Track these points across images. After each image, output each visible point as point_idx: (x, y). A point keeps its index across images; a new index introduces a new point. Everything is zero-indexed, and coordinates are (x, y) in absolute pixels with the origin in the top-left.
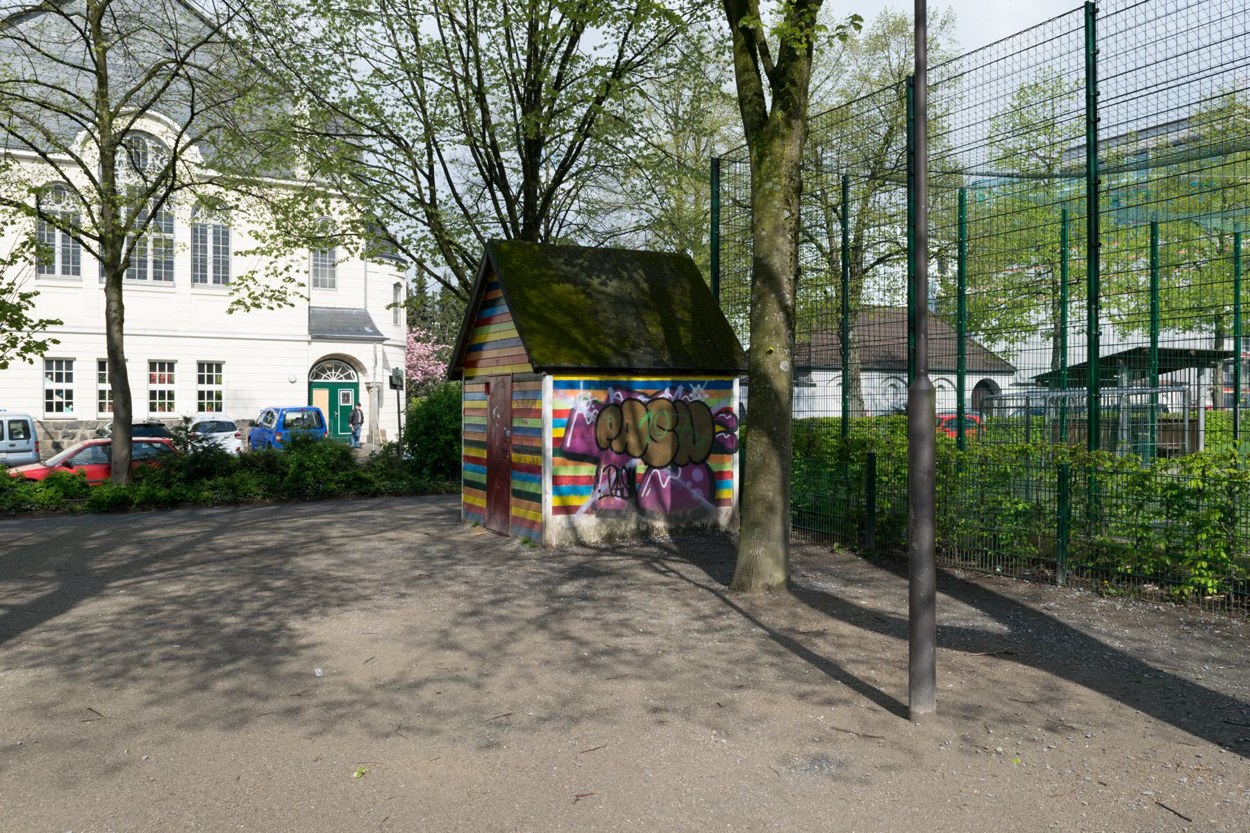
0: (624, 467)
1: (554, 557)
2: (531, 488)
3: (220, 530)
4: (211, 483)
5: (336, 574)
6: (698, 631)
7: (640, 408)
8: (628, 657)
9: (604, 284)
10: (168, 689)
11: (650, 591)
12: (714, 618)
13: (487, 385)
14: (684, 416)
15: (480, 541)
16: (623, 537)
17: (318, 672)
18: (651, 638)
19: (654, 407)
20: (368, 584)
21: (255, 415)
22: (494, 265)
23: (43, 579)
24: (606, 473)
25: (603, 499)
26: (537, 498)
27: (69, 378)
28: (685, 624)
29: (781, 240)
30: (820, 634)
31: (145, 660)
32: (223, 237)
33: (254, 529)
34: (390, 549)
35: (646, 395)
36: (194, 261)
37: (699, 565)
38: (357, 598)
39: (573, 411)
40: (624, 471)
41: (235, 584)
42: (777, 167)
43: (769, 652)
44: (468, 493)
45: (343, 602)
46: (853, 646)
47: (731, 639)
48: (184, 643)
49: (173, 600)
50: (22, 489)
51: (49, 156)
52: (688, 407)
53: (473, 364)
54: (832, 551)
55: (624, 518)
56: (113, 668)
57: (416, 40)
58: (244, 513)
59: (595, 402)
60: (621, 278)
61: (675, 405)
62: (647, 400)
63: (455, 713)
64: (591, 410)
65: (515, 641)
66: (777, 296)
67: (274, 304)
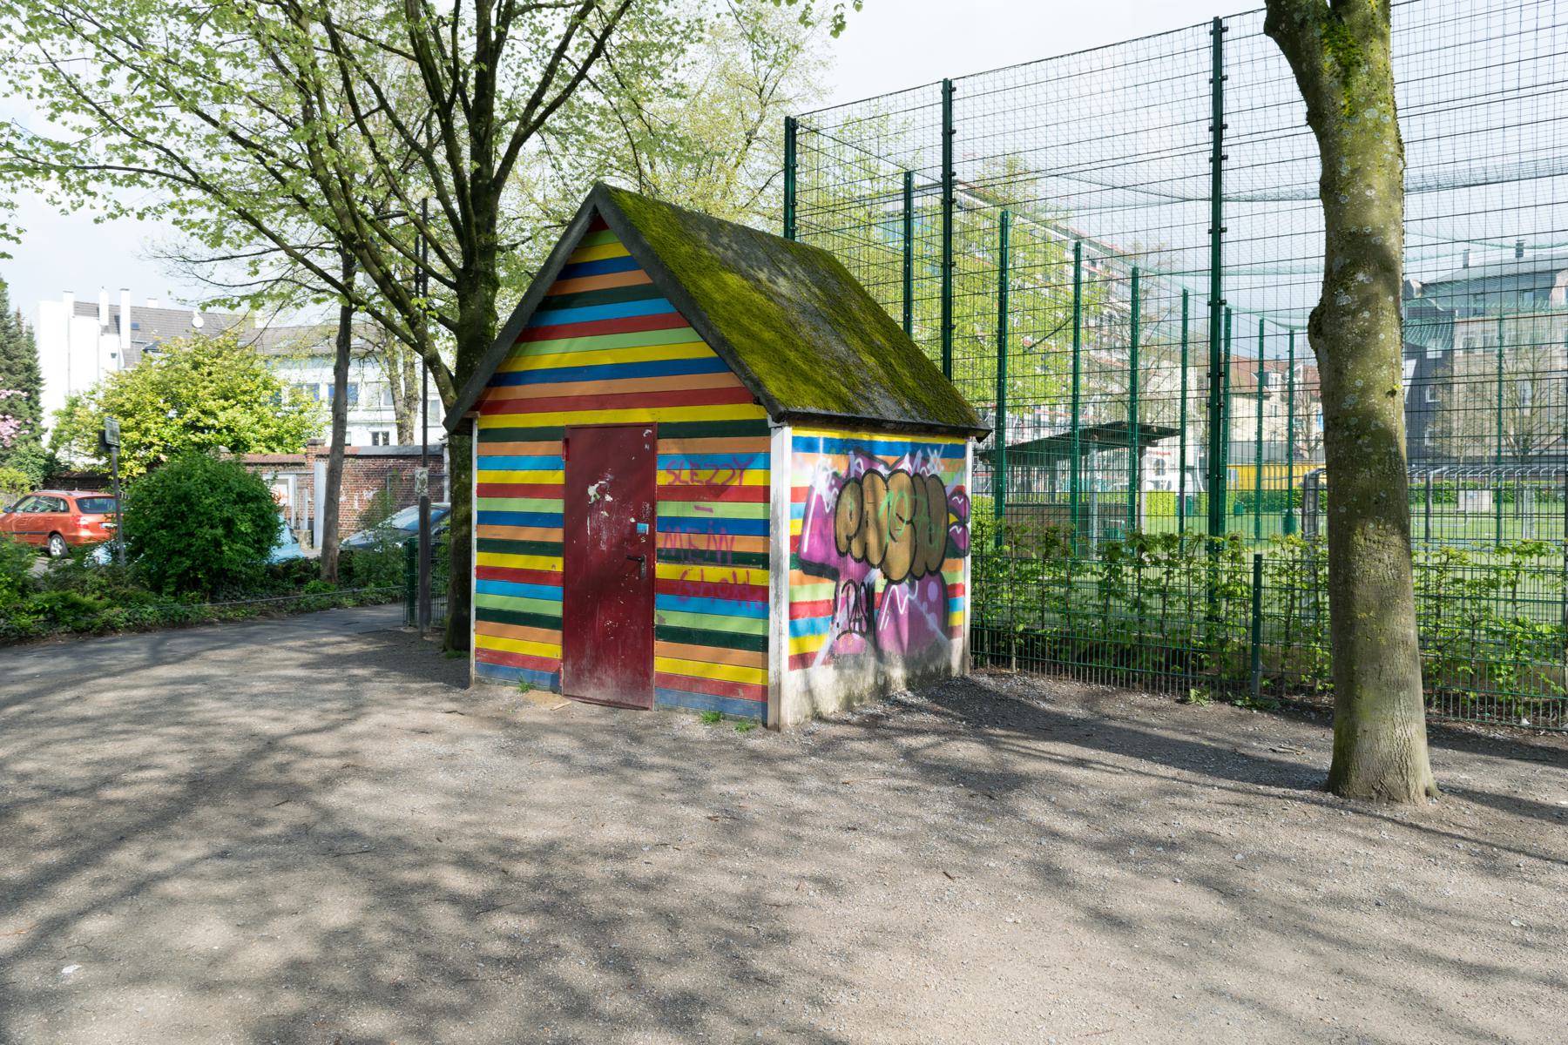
0: (863, 584)
39: (811, 488)
64: (831, 487)
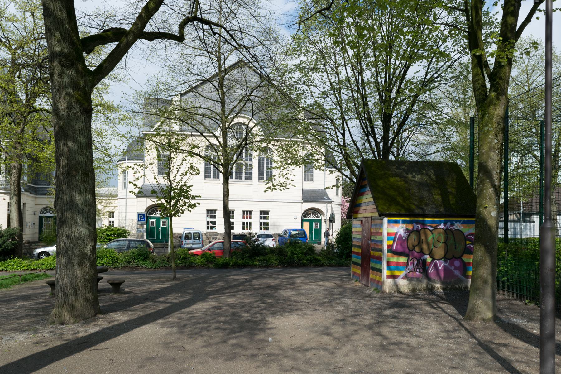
1: (387, 297)
2: (378, 266)
3: (256, 278)
4: (258, 258)
5: (293, 298)
6: (442, 338)
7: (429, 232)
8: (404, 347)
9: (414, 177)
10: (212, 341)
11: (425, 316)
12: (452, 332)
13: (362, 221)
15: (357, 288)
16: (420, 290)
17: (270, 340)
18: (418, 338)
19: (436, 232)
20: (304, 304)
21: (280, 232)
22: (364, 170)
23: (188, 293)
26: (380, 271)
27: (215, 217)
28: (437, 334)
29: (493, 154)
30: (505, 345)
31: (209, 328)
32: (270, 161)
33: (269, 278)
34: (318, 289)
35: (432, 227)
36: (259, 172)
37: (454, 306)
38: (297, 310)
39: (397, 233)
41: (253, 300)
42: (491, 119)
43: (475, 352)
44: (354, 267)
45: (291, 311)
46: (521, 353)
47: (458, 343)
48: (225, 323)
49: (228, 305)
50: (192, 258)
51: (204, 134)
53: (357, 212)
54: (525, 304)
55: (421, 282)
56: (197, 331)
57: (338, 77)
58: (269, 271)
59: (407, 229)
60: (422, 174)
61: (446, 231)
63: (318, 364)
64: (405, 233)
65: (356, 334)
67: (282, 188)
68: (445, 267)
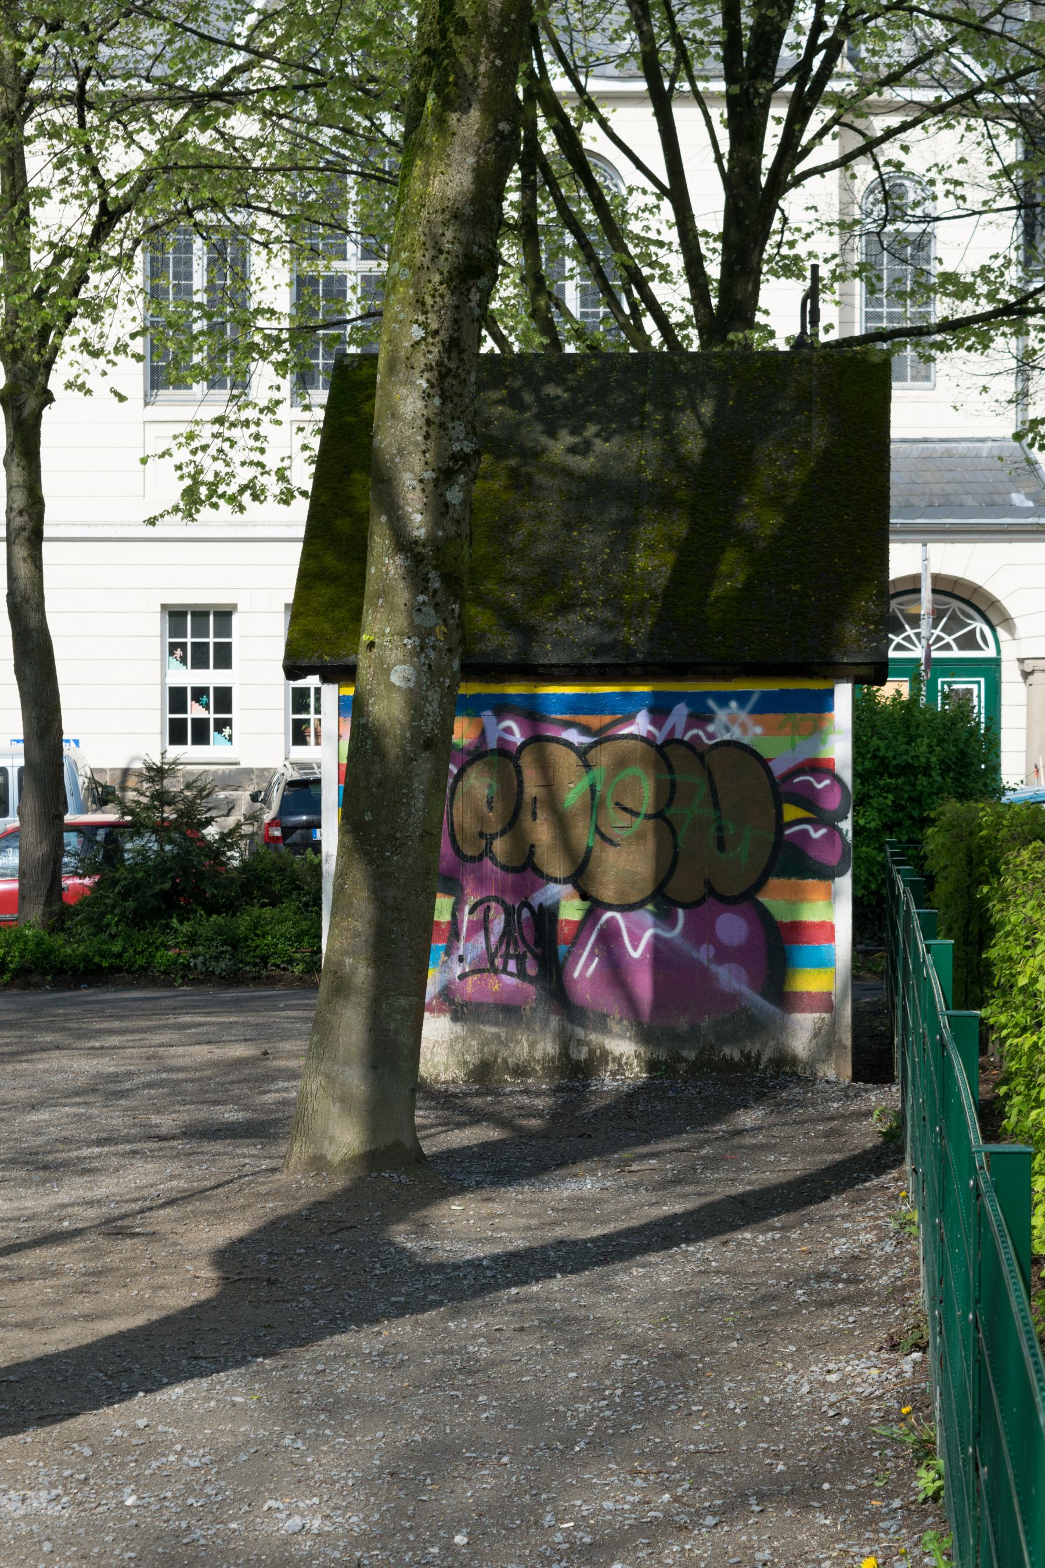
4: (186, 928)
14: (691, 779)
19: (603, 757)
24: (478, 915)
25: (470, 980)
27: (224, 658)
35: (585, 730)
40: (525, 913)
52: (701, 757)
62: (587, 740)
66: (390, 520)
68: (659, 950)
